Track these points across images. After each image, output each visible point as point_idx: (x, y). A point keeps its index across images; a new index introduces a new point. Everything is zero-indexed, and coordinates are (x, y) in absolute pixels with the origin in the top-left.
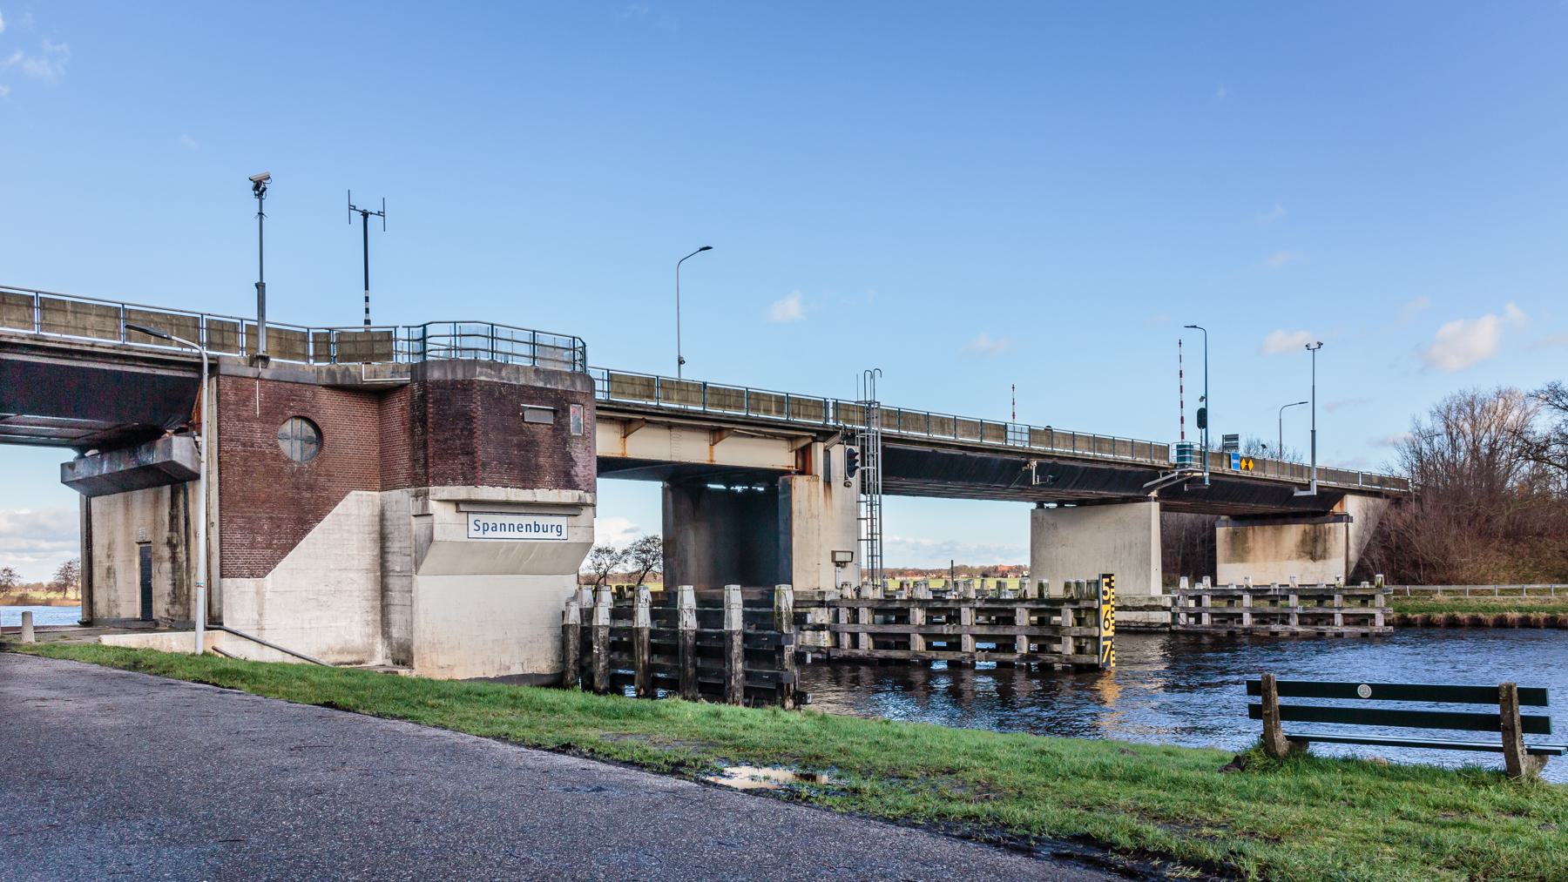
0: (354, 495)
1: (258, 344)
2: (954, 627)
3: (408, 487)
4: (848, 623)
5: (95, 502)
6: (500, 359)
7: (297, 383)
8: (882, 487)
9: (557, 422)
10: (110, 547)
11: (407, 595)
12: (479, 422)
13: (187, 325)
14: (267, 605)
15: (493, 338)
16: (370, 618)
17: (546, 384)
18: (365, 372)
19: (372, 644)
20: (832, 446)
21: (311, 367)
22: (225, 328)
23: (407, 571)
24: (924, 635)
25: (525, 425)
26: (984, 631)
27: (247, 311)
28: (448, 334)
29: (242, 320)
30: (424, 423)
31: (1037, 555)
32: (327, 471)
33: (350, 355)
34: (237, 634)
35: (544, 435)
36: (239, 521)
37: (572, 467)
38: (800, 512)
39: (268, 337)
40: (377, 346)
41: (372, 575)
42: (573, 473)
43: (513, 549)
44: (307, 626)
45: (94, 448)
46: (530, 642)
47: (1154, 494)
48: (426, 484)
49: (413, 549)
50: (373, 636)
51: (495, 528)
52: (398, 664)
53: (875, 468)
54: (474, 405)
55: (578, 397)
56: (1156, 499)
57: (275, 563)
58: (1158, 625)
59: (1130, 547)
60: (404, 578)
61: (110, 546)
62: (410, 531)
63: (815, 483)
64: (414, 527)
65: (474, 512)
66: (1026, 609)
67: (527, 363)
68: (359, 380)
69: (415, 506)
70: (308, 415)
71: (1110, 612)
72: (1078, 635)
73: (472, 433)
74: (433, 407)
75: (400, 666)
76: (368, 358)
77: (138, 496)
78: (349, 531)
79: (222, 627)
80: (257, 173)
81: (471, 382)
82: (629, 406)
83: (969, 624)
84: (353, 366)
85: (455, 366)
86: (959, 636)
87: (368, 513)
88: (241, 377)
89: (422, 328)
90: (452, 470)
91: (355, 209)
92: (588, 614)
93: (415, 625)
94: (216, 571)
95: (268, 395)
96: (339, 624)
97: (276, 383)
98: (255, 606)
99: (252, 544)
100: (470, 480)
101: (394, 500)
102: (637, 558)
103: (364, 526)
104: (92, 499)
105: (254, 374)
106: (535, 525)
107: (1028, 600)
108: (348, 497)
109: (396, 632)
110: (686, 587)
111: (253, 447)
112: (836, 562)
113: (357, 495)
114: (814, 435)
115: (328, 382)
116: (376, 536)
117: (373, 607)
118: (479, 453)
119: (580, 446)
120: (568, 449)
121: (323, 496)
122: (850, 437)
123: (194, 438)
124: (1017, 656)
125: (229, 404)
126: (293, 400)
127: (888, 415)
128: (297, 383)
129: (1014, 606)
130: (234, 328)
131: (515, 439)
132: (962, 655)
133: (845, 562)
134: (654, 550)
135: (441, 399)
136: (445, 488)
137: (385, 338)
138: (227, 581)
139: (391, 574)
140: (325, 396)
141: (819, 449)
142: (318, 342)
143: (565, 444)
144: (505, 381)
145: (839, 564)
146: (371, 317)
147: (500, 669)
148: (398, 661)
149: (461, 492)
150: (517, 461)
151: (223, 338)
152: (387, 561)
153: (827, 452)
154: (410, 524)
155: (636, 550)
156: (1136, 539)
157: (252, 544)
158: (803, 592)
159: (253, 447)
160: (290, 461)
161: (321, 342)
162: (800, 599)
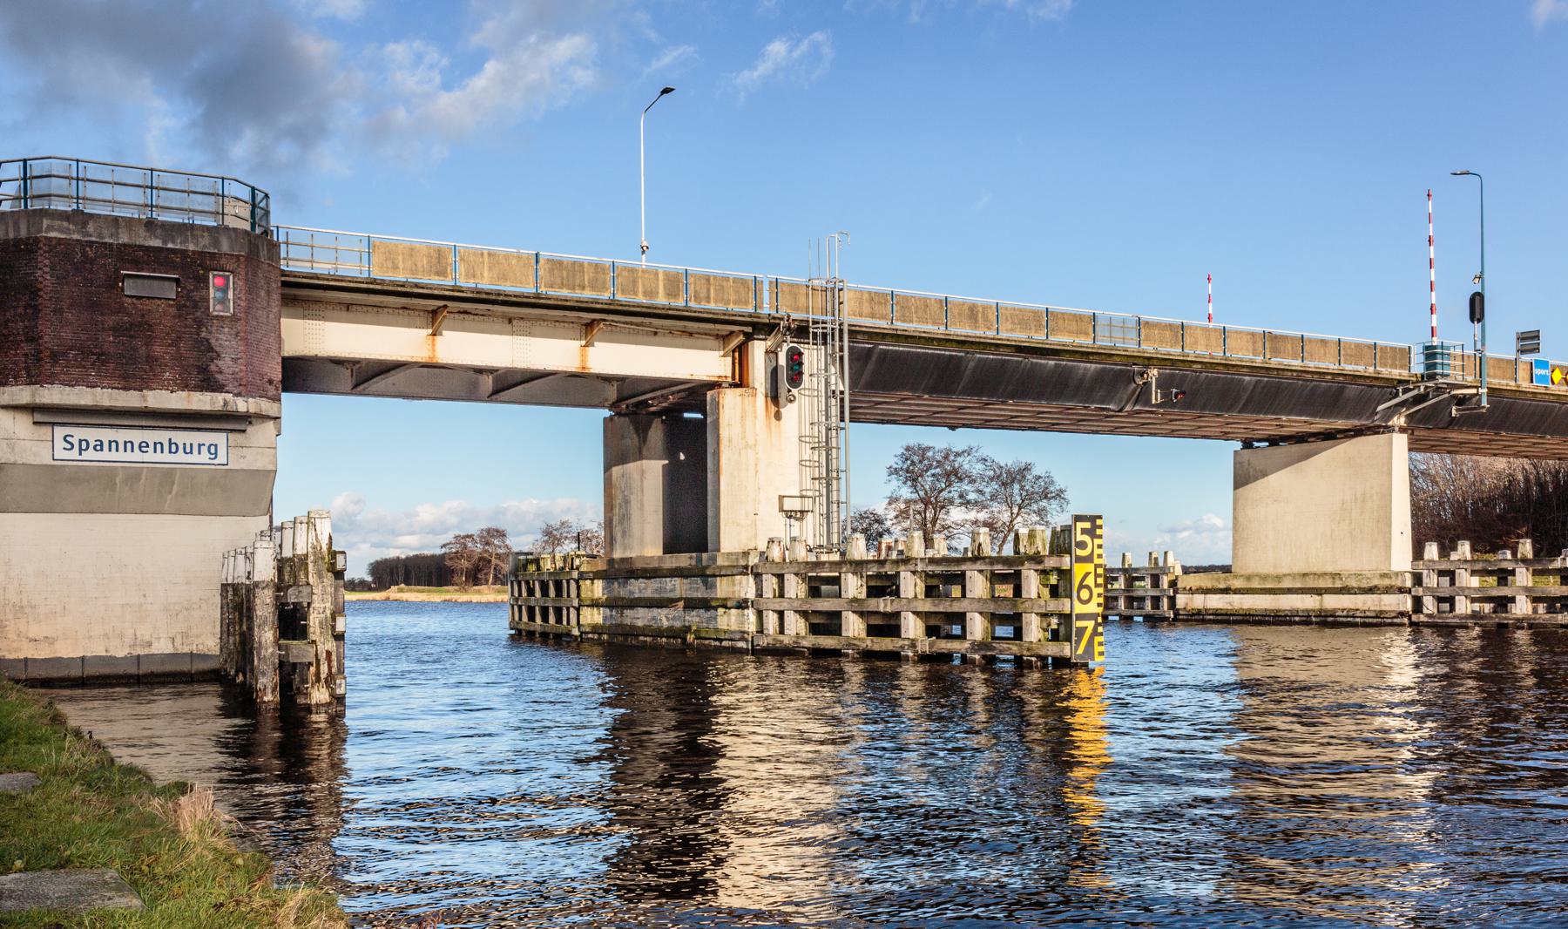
2: (892, 601)
4: (774, 597)
8: (852, 408)
17: (165, 242)
24: (861, 614)
31: (1240, 519)
37: (212, 360)
38: (730, 441)
42: (213, 367)
46: (187, 609)
47: (1399, 420)
51: (99, 446)
54: (40, 273)
55: (223, 261)
56: (1402, 430)
58: (1393, 615)
59: (1364, 501)
71: (1092, 577)
72: (1043, 611)
73: (36, 309)
81: (37, 240)
82: (403, 286)
85: (18, 219)
86: (897, 615)
90: (14, 363)
106: (170, 444)
107: (984, 558)
114: (749, 329)
118: (46, 338)
119: (226, 330)
120: (203, 334)
127: (872, 300)
129: (963, 567)
131: (111, 321)
132: (901, 643)
133: (802, 512)
136: (6, 388)
141: (758, 349)
144: (93, 239)
147: (135, 645)
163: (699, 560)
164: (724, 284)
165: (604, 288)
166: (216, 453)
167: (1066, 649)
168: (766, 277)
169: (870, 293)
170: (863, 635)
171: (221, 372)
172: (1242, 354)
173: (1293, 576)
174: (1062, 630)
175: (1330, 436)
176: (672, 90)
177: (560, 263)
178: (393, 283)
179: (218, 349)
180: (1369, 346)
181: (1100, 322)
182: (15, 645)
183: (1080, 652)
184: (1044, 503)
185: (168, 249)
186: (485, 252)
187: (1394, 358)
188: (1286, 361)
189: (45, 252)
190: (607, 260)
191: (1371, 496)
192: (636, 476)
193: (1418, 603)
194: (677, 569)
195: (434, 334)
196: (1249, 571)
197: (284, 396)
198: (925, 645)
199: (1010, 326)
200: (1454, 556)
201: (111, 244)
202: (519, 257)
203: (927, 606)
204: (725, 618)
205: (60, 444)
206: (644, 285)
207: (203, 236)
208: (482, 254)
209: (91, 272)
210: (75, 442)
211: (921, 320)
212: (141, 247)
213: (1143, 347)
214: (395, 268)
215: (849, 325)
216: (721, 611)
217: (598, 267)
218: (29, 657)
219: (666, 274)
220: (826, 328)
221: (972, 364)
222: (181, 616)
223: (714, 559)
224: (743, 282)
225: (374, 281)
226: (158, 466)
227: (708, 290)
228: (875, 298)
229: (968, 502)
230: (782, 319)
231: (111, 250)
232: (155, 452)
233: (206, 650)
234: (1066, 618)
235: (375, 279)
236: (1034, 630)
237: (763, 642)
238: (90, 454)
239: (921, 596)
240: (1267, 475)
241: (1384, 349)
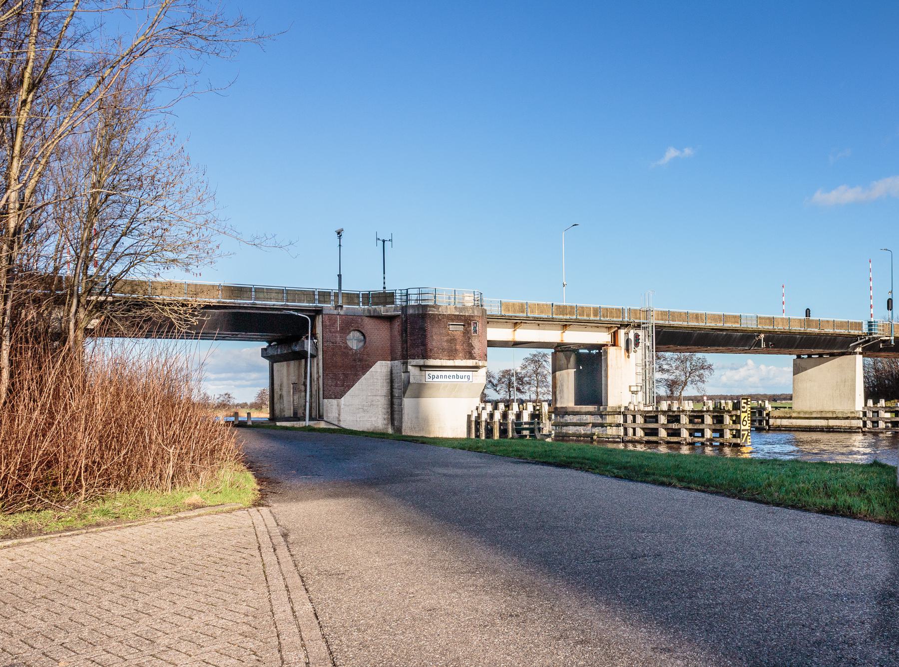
5: (275, 365)
10: (281, 386)
13: (309, 295)
14: (342, 411)
18: (382, 310)
21: (361, 308)
24: (665, 429)
27: (333, 286)
36: (331, 375)
42: (473, 352)
44: (358, 420)
45: (274, 341)
47: (859, 350)
51: (438, 377)
55: (475, 318)
56: (860, 353)
59: (845, 382)
61: (281, 385)
62: (401, 379)
70: (360, 329)
71: (747, 417)
76: (385, 304)
77: (292, 363)
78: (377, 379)
80: (338, 229)
81: (426, 314)
86: (679, 429)
94: (321, 396)
95: (342, 322)
98: (337, 412)
104: (274, 364)
108: (376, 364)
109: (396, 423)
114: (619, 326)
115: (368, 315)
116: (389, 381)
117: (387, 412)
132: (681, 439)
138: (326, 400)
141: (622, 332)
146: (386, 286)
149: (421, 362)
160: (352, 349)
163: (599, 409)
165: (573, 314)
167: (738, 441)
170: (666, 436)
173: (817, 412)
174: (737, 434)
175: (833, 355)
177: (560, 306)
178: (508, 316)
180: (846, 322)
181: (742, 318)
183: (743, 441)
184: (702, 371)
187: (856, 327)
188: (813, 330)
190: (574, 305)
192: (566, 375)
193: (865, 423)
194: (588, 412)
196: (799, 410)
198: (689, 439)
200: (879, 405)
202: (547, 305)
203: (690, 426)
204: (611, 430)
211: (679, 321)
214: (509, 310)
216: (608, 427)
217: (571, 307)
219: (594, 308)
221: (695, 335)
223: (606, 409)
224: (619, 310)
225: (503, 316)
228: (663, 314)
229: (663, 370)
234: (738, 431)
236: (728, 435)
237: (627, 439)
239: (688, 423)
241: (852, 323)
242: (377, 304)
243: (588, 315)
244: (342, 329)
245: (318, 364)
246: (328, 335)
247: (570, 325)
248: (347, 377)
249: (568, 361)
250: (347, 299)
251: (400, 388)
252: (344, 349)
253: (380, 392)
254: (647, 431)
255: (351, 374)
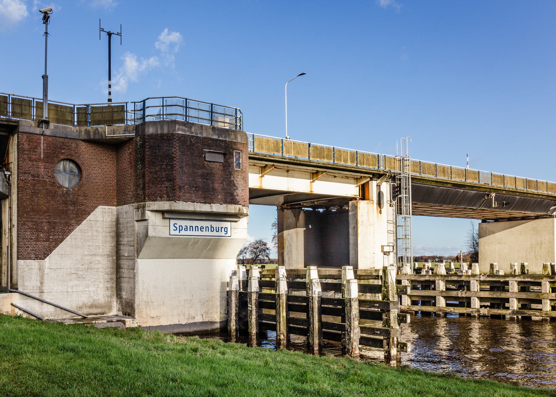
0: (100, 209)
1: (43, 114)
3: (133, 203)
6: (191, 121)
7: (67, 138)
9: (226, 161)
11: (132, 271)
12: (177, 161)
14: (46, 277)
15: (186, 108)
16: (109, 286)
17: (219, 137)
18: (107, 131)
19: (110, 302)
20: (381, 183)
22: (23, 104)
23: (131, 256)
25: (206, 163)
26: (486, 294)
28: (159, 105)
29: (34, 99)
30: (143, 160)
32: (84, 193)
33: (99, 121)
34: (26, 295)
35: (217, 169)
36: (29, 224)
37: (235, 190)
38: (362, 222)
39: (49, 109)
40: (115, 115)
41: (111, 258)
42: (235, 194)
43: (197, 242)
44: (70, 290)
46: (207, 301)
48: (144, 200)
49: (136, 242)
50: (111, 297)
52: (126, 315)
53: (408, 196)
55: (238, 146)
57: (51, 251)
59: (541, 244)
60: (130, 260)
62: (134, 230)
63: (371, 205)
64: (136, 228)
65: (173, 219)
66: (516, 281)
67: (208, 124)
68: (104, 136)
69: (137, 215)
70: (73, 158)
73: (172, 167)
74: (149, 151)
75: (127, 316)
76: (110, 122)
79: (17, 291)
81: (173, 135)
82: (266, 156)
83: (476, 291)
84: (100, 127)
87: (109, 220)
88: (32, 133)
89: (143, 102)
90: (161, 191)
91: (103, 31)
92: (246, 284)
93: (136, 291)
95: (48, 146)
96: (90, 289)
97: (54, 138)
98: (38, 278)
99: (37, 239)
100: (172, 197)
101: (125, 211)
102: (252, 251)
103: (106, 228)
105: (40, 132)
106: (211, 227)
108: (97, 210)
109: (124, 295)
110: (348, 267)
111: (39, 177)
112: (384, 252)
113: (103, 208)
114: (371, 176)
115: (86, 138)
116: (113, 234)
117: (111, 279)
119: (240, 176)
121: (81, 209)
122: (393, 178)
123: (4, 172)
124: (510, 311)
125: (24, 151)
126: (64, 149)
128: (67, 138)
129: (507, 279)
130: (28, 103)
131: (200, 172)
132: (471, 310)
133: (389, 252)
134: (260, 247)
135: (154, 146)
136: (156, 202)
137: (120, 109)
138: (21, 262)
139: (122, 258)
140: (83, 146)
141: (373, 184)
142: (79, 113)
143: (230, 175)
144: (194, 135)
145: (385, 253)
148: (126, 313)
149: (165, 205)
150: (200, 185)
151: (22, 111)
152: (120, 250)
153: (379, 186)
154: (134, 226)
155: (251, 247)
156: (545, 239)
157: (37, 239)
158: (365, 270)
159: (39, 177)
160: (61, 187)
161: (82, 113)
162: (363, 274)
164: (369, 157)
166: (227, 231)
168: (382, 155)
169: (413, 162)
170: (445, 306)
171: (238, 196)
172: (521, 188)
175: (525, 218)
176: (305, 74)
177: (317, 147)
178: (262, 155)
179: (237, 185)
182: (145, 320)
185: (220, 140)
186: (292, 142)
189: (177, 140)
191: (545, 243)
195: (262, 177)
197: (250, 205)
199: (455, 176)
201: (200, 137)
205: (172, 228)
206: (343, 157)
207: (232, 134)
208: (291, 143)
209: (193, 149)
210: (178, 226)
212: (210, 139)
213: (493, 184)
214: (262, 148)
215: (411, 175)
218: (151, 325)
219: (351, 153)
220: (401, 176)
222: (205, 304)
225: (256, 154)
226: (207, 237)
227: (364, 160)
230: (387, 172)
231: (200, 140)
232: (206, 231)
233: (214, 319)
235: (256, 153)
238: (183, 232)
240: (495, 233)
242: (99, 123)
243: (346, 161)
244: (47, 156)
245: (10, 208)
246: (27, 165)
247: (322, 172)
248: (54, 228)
249: (297, 218)
250: (57, 114)
251: (132, 243)
252: (51, 185)
253: (101, 250)
254: (414, 299)
255: (60, 223)
